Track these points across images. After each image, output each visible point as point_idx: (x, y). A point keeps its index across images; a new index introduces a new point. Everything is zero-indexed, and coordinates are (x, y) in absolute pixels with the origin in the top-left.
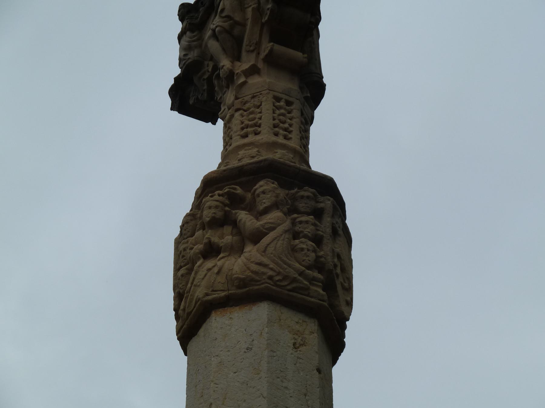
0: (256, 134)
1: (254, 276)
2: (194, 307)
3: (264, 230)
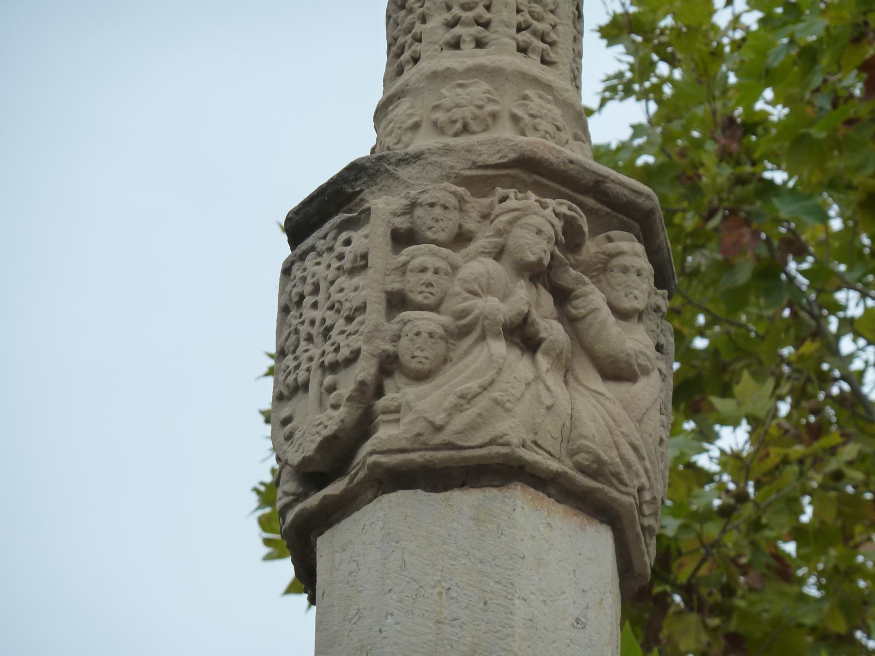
0: (480, 44)
1: (622, 469)
2: (481, 446)
3: (636, 367)
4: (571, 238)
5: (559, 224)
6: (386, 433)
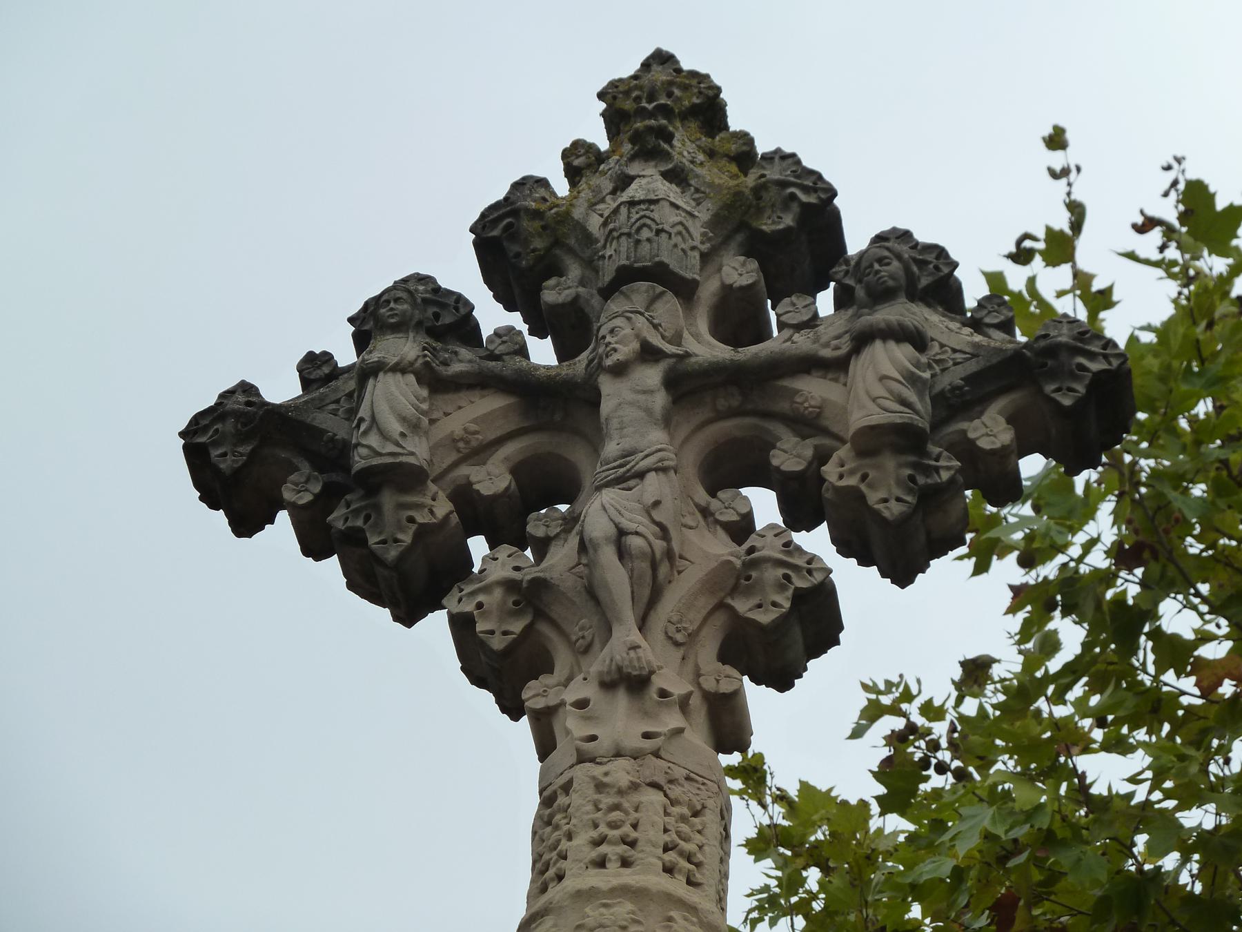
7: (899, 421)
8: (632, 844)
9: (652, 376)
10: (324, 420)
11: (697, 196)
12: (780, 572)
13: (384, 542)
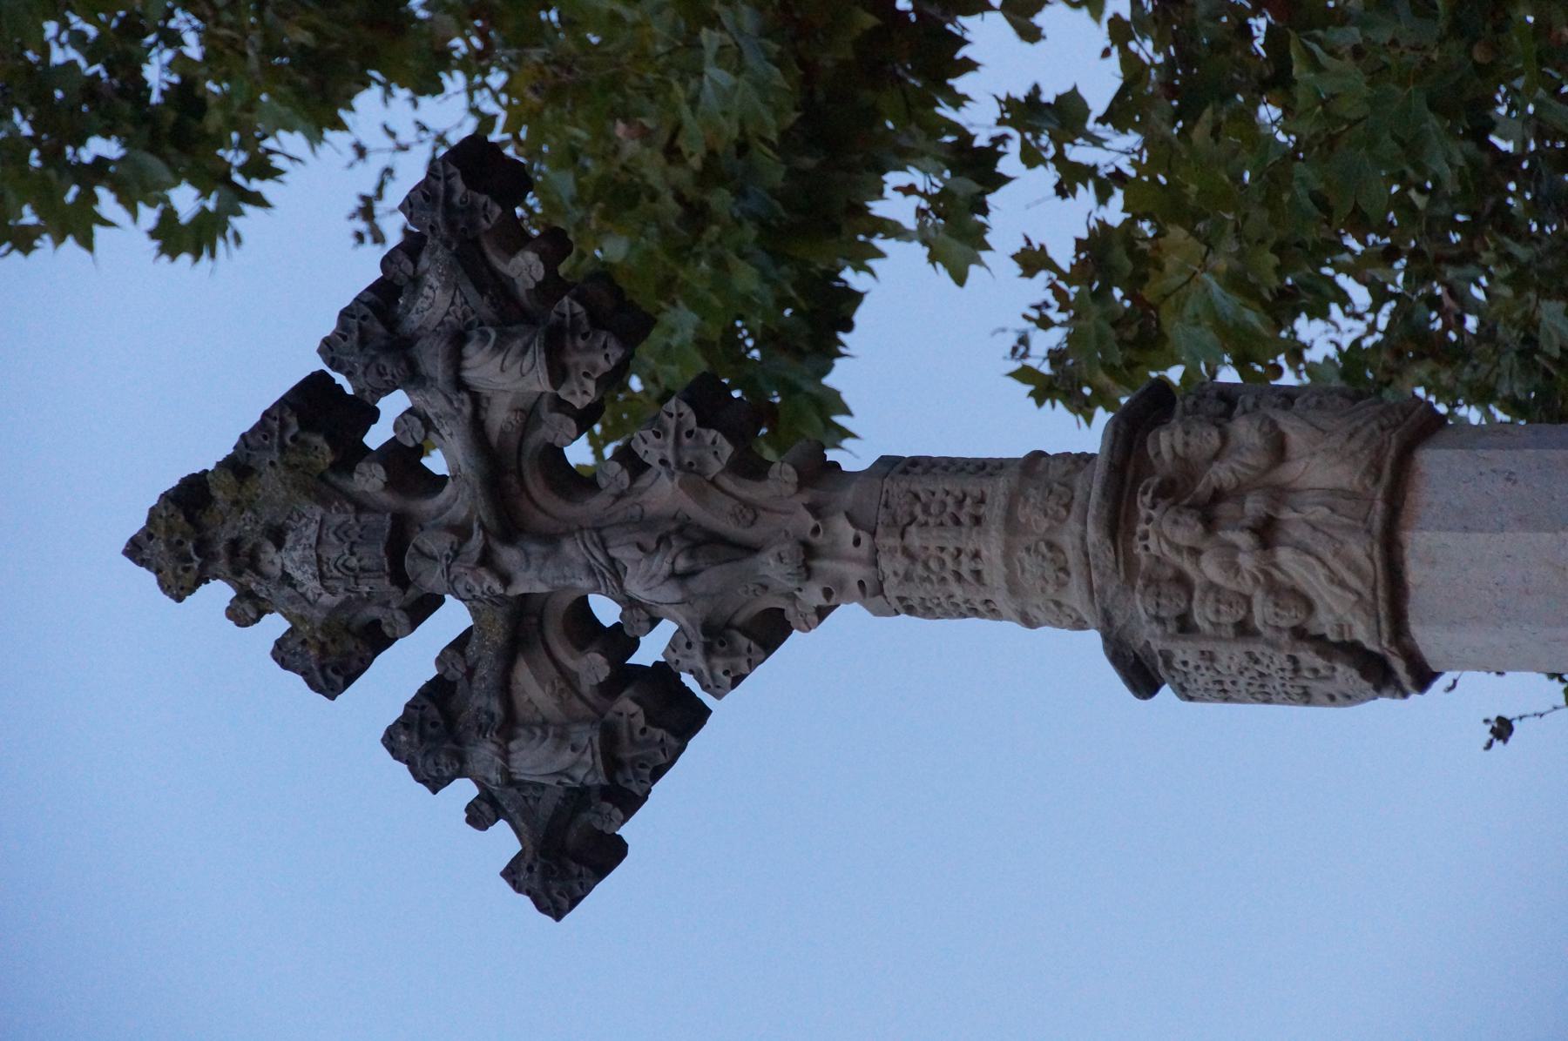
4: (1169, 492)
5: (1162, 504)
6: (1361, 632)
7: (543, 355)
8: (959, 551)
9: (509, 556)
10: (547, 807)
11: (295, 517)
12: (686, 441)
13: (664, 751)
